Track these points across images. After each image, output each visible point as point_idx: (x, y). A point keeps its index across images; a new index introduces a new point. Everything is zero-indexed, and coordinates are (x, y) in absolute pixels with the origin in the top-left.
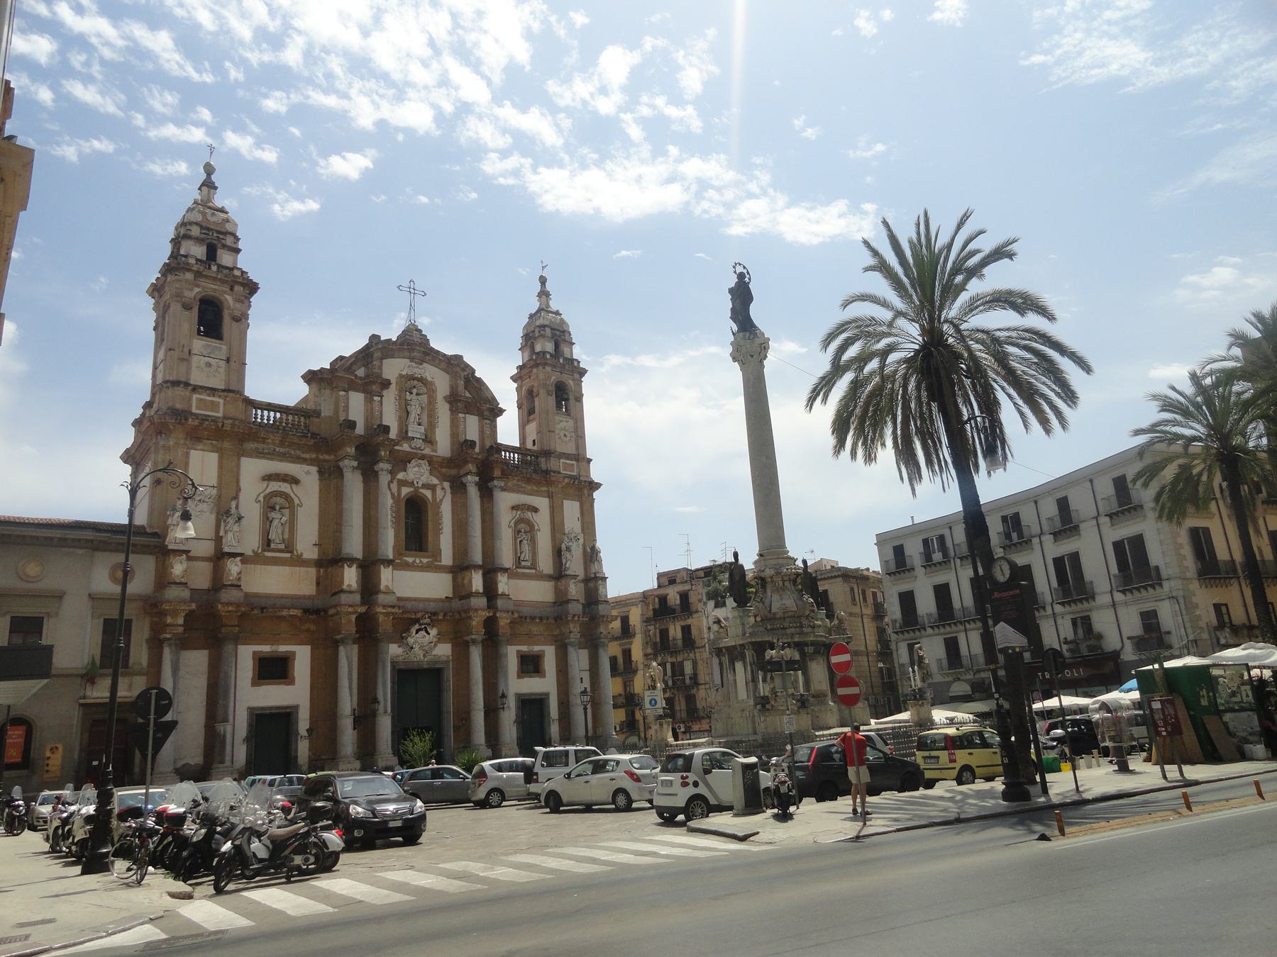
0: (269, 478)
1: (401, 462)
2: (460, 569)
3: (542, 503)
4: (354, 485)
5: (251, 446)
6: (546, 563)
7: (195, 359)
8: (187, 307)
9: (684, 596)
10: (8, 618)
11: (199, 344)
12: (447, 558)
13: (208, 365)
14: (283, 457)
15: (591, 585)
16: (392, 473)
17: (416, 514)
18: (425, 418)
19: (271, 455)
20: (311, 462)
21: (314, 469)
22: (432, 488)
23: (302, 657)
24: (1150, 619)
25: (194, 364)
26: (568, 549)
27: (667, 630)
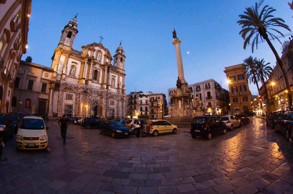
0: (73, 62)
1: (95, 63)
2: (102, 84)
3: (117, 76)
4: (86, 66)
5: (71, 56)
6: (116, 86)
7: (65, 40)
8: (66, 32)
9: (135, 96)
10: (29, 80)
11: (67, 38)
12: (100, 82)
13: (67, 42)
14: (75, 59)
15: (123, 91)
16: (93, 65)
17: (96, 72)
18: (100, 58)
19: (74, 59)
20: (80, 61)
21: (80, 62)
22: (99, 69)
23: (74, 96)
24: (210, 104)
25: (65, 41)
26: (120, 84)
27: (132, 101)
